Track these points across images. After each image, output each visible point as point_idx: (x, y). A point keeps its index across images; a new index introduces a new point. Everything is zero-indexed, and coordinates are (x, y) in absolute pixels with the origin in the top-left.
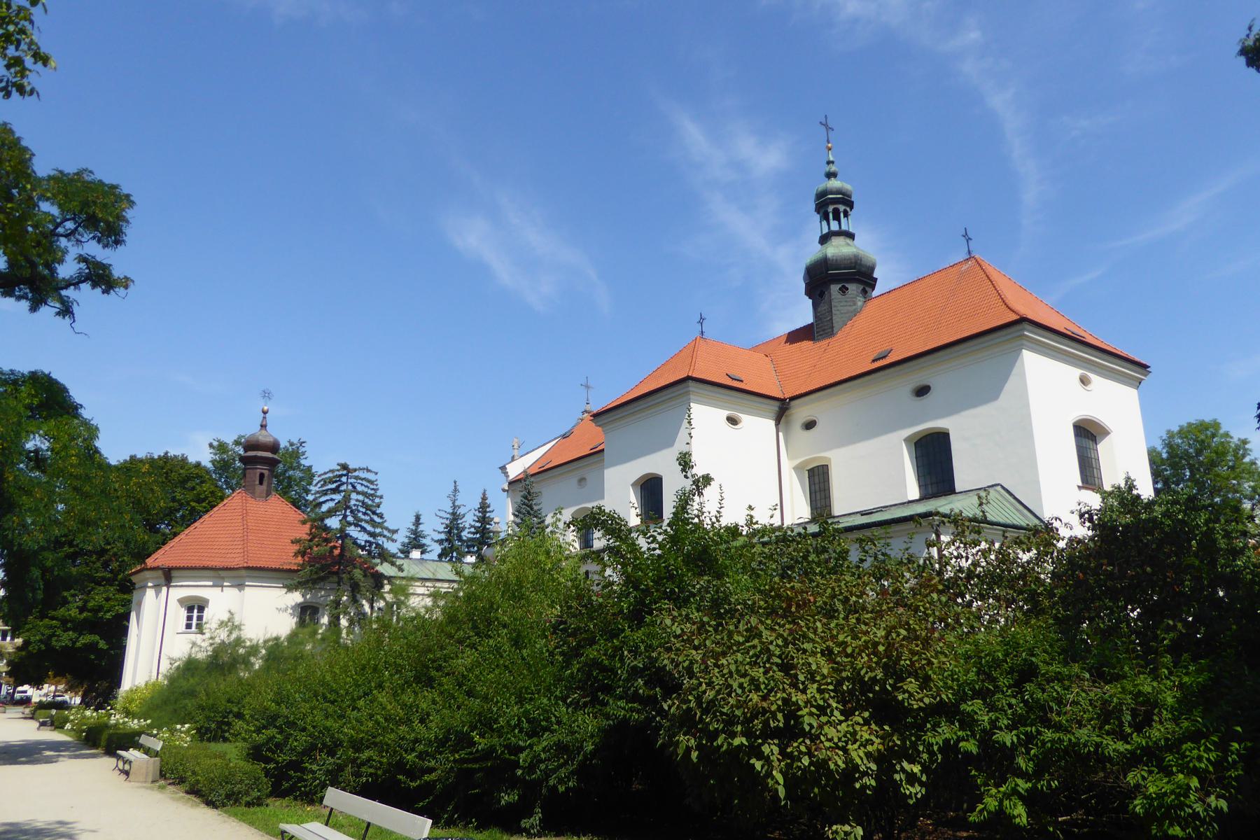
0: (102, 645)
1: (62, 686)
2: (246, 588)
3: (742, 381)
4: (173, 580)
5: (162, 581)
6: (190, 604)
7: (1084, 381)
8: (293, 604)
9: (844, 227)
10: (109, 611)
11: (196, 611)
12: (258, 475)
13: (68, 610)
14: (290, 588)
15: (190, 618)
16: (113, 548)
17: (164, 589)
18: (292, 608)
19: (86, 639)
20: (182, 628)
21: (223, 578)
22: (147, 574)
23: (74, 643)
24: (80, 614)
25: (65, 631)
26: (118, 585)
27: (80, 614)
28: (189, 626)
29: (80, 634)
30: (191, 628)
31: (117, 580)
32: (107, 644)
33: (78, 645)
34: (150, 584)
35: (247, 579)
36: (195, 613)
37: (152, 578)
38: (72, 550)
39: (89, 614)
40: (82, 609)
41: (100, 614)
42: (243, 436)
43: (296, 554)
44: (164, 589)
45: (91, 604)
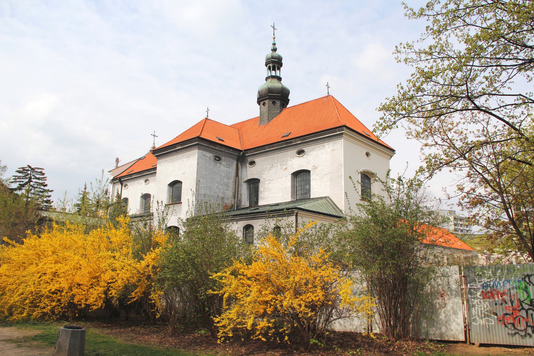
7: (367, 154)
9: (278, 75)
36: (393, 301)
43: (114, 179)
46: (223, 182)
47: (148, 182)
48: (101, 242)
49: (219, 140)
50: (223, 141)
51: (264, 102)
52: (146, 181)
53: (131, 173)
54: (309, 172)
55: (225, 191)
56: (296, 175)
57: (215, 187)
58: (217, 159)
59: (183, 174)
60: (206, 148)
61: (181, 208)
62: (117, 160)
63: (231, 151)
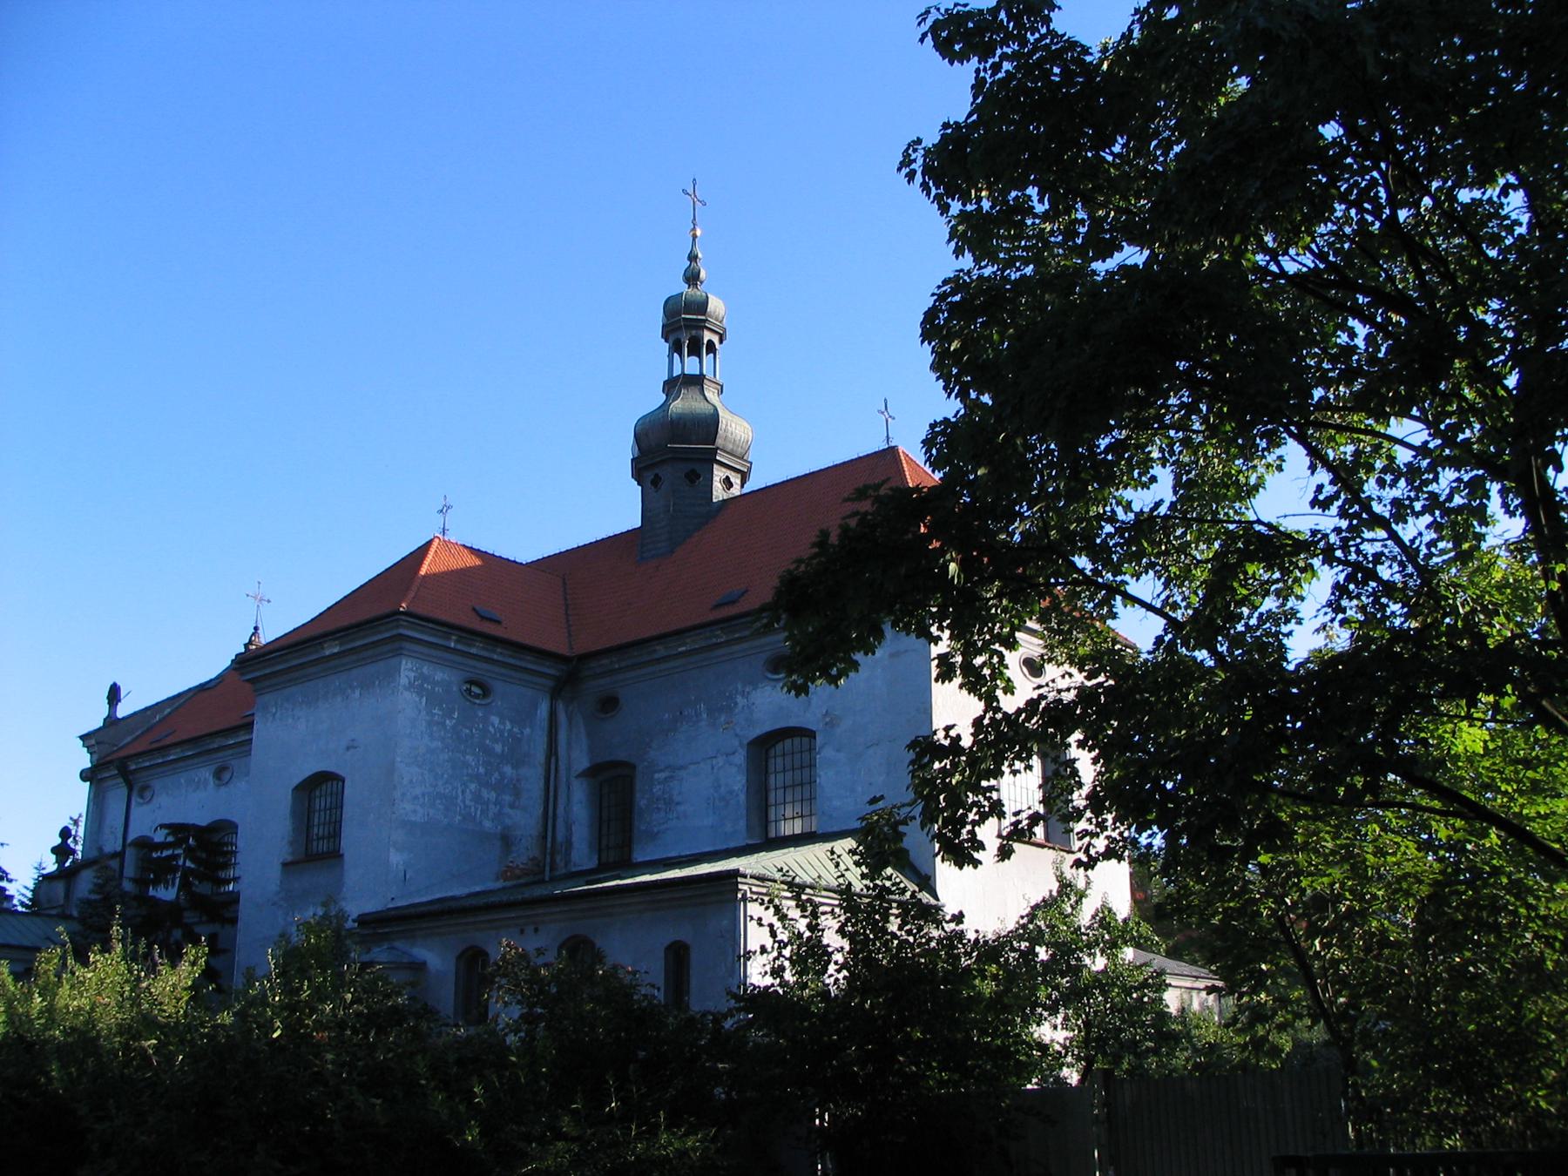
46: (496, 775)
47: (226, 776)
48: (419, 759)
49: (483, 618)
50: (499, 622)
51: (656, 475)
52: (218, 774)
53: (168, 741)
54: (811, 734)
55: (507, 810)
56: (764, 746)
57: (468, 796)
58: (476, 690)
59: (348, 748)
60: (434, 652)
61: (342, 867)
62: (114, 695)
63: (529, 663)
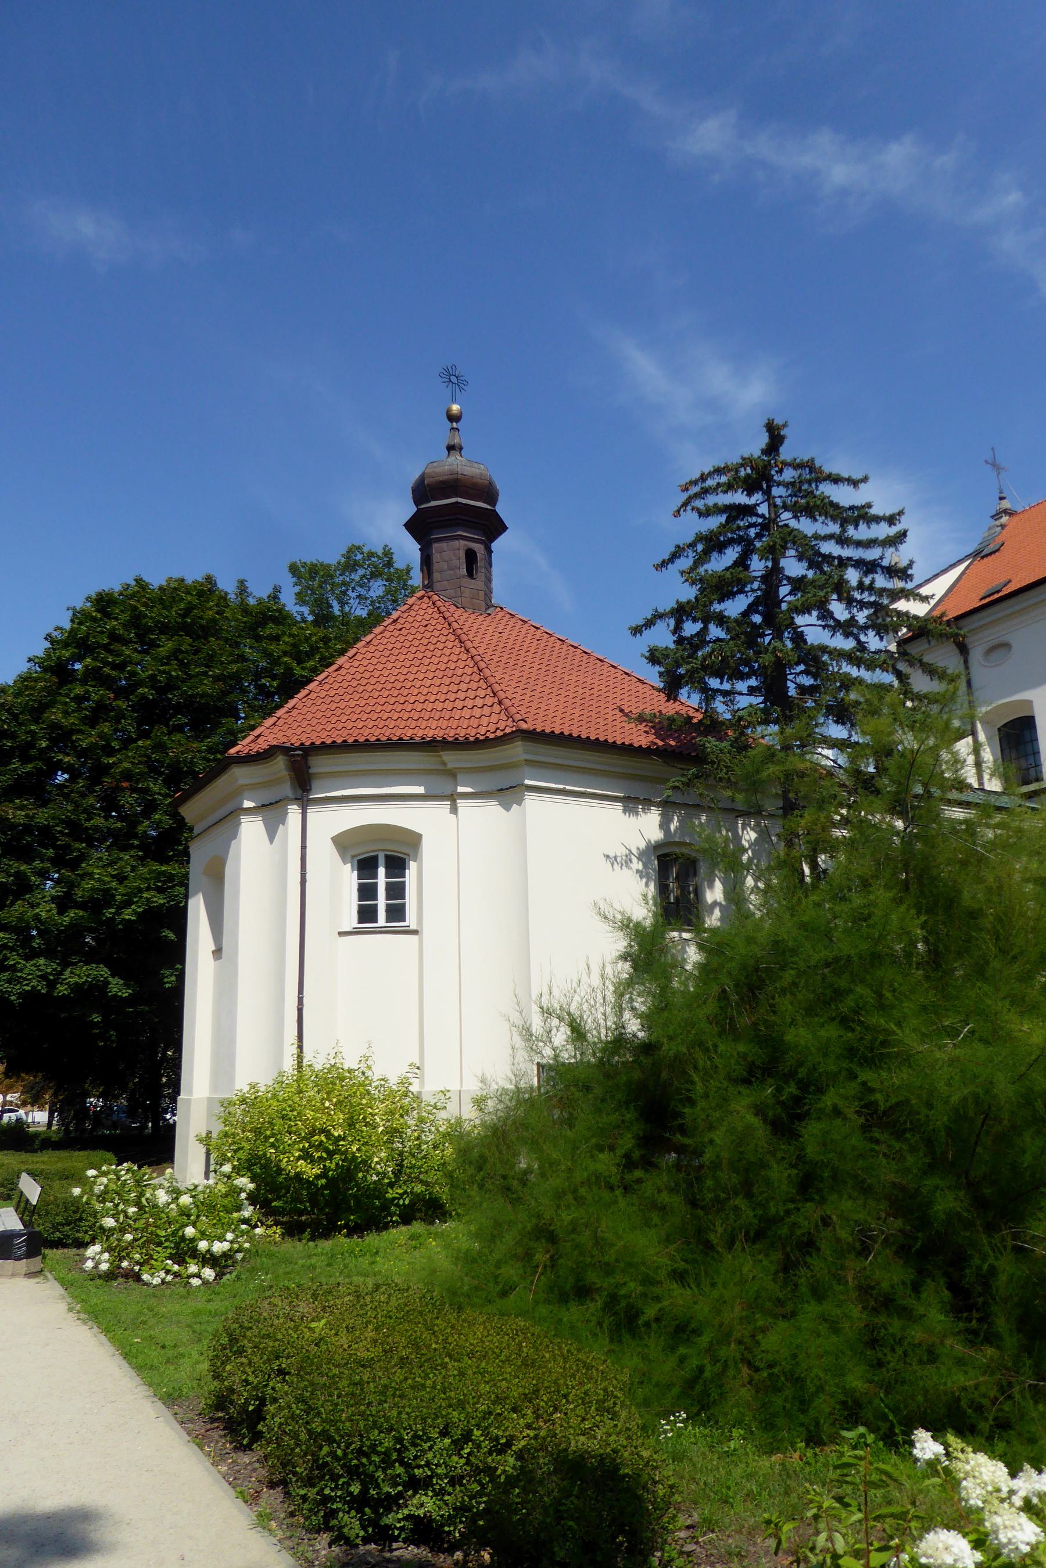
0: (117, 987)
1: (17, 1095)
2: (531, 801)
3: (1010, 581)
4: (315, 784)
5: (287, 789)
6: (365, 851)
8: (643, 845)
10: (128, 904)
11: (381, 871)
12: (462, 554)
13: (32, 906)
14: (632, 803)
15: (367, 892)
16: (120, 761)
17: (294, 812)
18: (642, 855)
19: (80, 974)
20: (351, 920)
21: (452, 775)
22: (240, 775)
23: (52, 985)
24: (61, 913)
25: (27, 958)
26: (139, 848)
27: (61, 913)
28: (367, 914)
29: (65, 964)
30: (375, 920)
31: (135, 836)
32: (127, 985)
33: (62, 990)
34: (248, 804)
35: (527, 770)
37: (254, 787)
38: (29, 767)
39: (81, 913)
40: (63, 903)
41: (109, 912)
42: (359, 548)
44: (294, 812)
45: (79, 894)
